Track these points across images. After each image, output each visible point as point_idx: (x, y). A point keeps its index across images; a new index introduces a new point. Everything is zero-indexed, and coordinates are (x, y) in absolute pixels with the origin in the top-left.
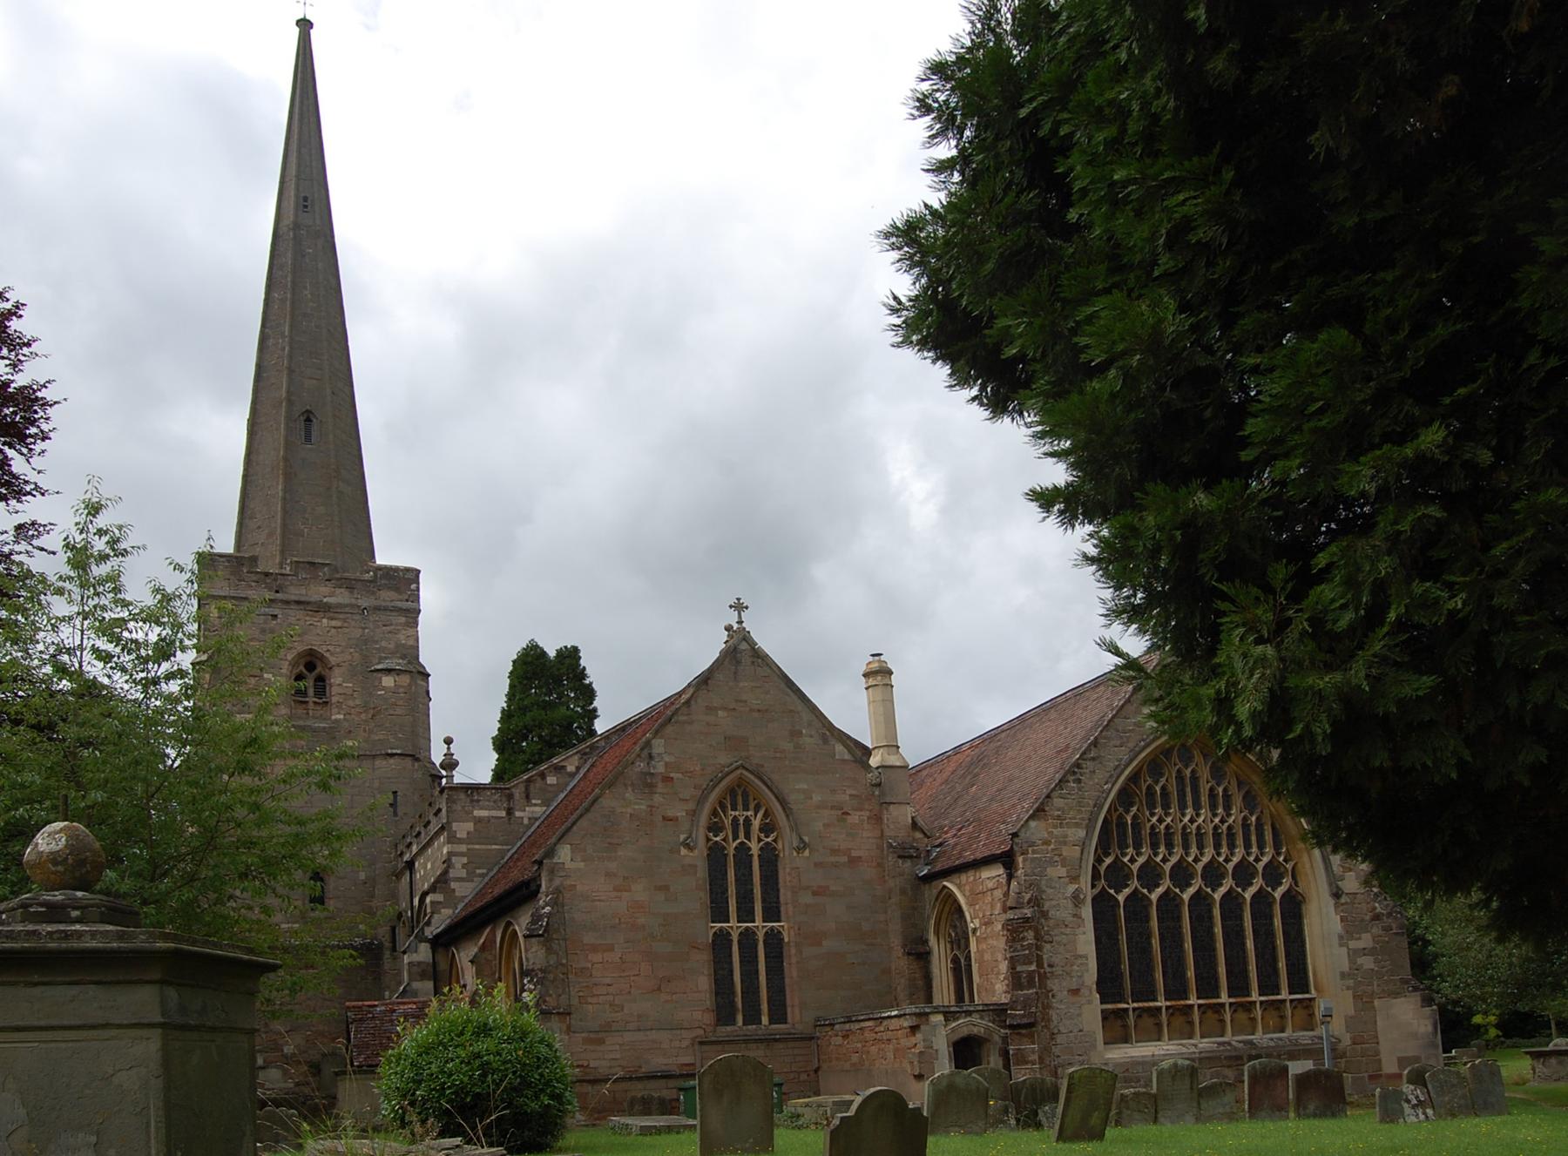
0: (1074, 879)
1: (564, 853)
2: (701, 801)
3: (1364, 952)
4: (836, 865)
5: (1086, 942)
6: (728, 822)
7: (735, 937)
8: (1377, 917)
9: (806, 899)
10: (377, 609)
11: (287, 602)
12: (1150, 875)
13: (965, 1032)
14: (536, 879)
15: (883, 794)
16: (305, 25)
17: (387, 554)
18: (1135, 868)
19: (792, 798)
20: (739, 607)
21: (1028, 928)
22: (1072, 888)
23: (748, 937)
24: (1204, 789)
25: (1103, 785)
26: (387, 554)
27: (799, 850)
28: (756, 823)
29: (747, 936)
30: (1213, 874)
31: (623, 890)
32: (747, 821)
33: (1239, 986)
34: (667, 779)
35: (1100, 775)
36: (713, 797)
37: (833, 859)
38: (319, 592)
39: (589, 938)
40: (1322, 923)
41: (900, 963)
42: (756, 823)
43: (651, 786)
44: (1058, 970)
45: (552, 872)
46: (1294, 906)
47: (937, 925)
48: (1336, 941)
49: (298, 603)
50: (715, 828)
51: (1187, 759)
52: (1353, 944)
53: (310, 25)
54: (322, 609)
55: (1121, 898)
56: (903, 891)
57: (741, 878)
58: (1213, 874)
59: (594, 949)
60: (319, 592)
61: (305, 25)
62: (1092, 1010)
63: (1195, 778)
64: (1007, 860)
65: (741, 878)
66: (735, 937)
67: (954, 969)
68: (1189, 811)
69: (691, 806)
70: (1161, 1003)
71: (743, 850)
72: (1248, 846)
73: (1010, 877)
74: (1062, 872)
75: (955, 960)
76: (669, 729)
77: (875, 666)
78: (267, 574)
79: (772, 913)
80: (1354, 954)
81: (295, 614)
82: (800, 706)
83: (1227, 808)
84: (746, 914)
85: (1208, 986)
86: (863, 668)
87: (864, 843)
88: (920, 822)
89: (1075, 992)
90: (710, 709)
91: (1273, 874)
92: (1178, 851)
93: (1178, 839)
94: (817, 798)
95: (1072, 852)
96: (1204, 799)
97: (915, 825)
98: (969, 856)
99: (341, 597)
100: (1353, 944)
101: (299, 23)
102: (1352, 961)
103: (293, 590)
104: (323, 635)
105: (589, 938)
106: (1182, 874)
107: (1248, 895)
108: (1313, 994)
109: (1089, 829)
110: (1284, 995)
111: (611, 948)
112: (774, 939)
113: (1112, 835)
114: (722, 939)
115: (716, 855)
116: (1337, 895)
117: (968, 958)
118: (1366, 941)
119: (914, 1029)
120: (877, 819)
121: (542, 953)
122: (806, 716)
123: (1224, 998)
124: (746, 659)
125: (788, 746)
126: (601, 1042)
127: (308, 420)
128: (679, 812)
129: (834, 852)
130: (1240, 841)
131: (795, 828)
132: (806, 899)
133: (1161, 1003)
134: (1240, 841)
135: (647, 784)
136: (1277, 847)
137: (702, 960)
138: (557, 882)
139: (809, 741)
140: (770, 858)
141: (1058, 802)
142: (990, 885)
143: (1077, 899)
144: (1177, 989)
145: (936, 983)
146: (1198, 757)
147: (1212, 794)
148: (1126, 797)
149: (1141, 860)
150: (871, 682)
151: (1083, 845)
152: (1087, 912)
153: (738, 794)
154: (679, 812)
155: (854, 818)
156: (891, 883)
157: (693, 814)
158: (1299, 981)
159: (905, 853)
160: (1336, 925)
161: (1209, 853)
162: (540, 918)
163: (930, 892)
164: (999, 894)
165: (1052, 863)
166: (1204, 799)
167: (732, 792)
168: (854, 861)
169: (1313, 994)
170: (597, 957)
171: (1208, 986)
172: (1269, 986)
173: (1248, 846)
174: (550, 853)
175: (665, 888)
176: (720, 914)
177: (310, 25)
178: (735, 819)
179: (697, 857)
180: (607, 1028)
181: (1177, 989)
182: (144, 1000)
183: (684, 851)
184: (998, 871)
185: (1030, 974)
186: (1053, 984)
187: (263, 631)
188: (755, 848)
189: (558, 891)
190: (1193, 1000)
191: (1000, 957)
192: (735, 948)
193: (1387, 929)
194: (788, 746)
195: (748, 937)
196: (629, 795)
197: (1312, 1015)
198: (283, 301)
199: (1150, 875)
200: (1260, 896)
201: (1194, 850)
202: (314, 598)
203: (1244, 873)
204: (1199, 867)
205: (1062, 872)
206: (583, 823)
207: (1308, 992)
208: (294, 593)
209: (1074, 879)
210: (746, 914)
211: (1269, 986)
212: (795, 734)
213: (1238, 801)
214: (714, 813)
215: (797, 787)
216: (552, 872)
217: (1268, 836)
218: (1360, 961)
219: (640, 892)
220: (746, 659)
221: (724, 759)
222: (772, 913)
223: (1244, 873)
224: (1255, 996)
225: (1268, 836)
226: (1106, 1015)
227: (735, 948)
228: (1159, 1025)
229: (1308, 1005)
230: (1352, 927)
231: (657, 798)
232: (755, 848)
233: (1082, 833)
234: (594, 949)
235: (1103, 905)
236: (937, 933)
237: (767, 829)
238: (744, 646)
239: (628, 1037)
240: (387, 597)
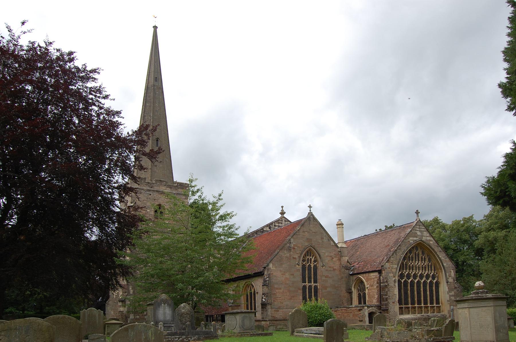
0: (394, 277)
1: (271, 265)
2: (301, 254)
3: (452, 296)
4: (330, 270)
5: (396, 291)
6: (307, 259)
7: (307, 287)
8: (456, 288)
9: (324, 278)
10: (178, 194)
11: (154, 191)
12: (409, 276)
13: (371, 311)
14: (263, 271)
15: (341, 254)
16: (155, 28)
17: (179, 177)
18: (406, 274)
19: (321, 254)
20: (310, 207)
21: (382, 288)
22: (394, 279)
23: (310, 287)
24: (420, 256)
25: (401, 255)
26: (179, 177)
27: (322, 266)
28: (313, 260)
29: (310, 286)
30: (421, 276)
31: (283, 274)
32: (311, 259)
33: (426, 303)
34: (294, 248)
35: (401, 253)
36: (304, 253)
37: (330, 269)
38: (162, 188)
39: (276, 286)
40: (444, 288)
41: (344, 293)
42: (313, 260)
43: (290, 250)
44: (390, 297)
45: (268, 270)
46: (437, 284)
47: (355, 285)
48: (447, 293)
49: (157, 191)
50: (303, 261)
51: (417, 250)
52: (450, 294)
53: (157, 27)
54: (162, 193)
55: (402, 281)
56: (346, 277)
57: (309, 273)
58: (421, 276)
59: (277, 289)
60: (162, 188)
61: (155, 28)
62: (397, 307)
63: (418, 254)
64: (380, 272)
65: (309, 273)
66: (307, 287)
67: (358, 296)
68: (417, 262)
69: (299, 255)
70: (410, 306)
71: (310, 266)
72: (429, 270)
73: (380, 276)
74: (392, 275)
75: (359, 295)
76: (295, 236)
77: (340, 223)
78: (149, 183)
79: (315, 282)
80: (450, 296)
81: (156, 195)
82: (324, 232)
83: (425, 261)
84: (310, 282)
85: (419, 303)
86: (336, 223)
87: (337, 266)
88: (349, 261)
89: (394, 303)
90: (304, 232)
91: (434, 277)
92: (414, 271)
93: (414, 268)
94: (327, 254)
95: (394, 270)
96: (420, 259)
97: (348, 262)
98: (365, 270)
99: (168, 190)
100: (450, 294)
101: (153, 27)
102: (450, 298)
103: (155, 187)
104: (162, 200)
105: (276, 286)
106: (415, 276)
107: (409, 281)
108: (441, 305)
109: (398, 265)
110: (435, 305)
111: (280, 289)
112: (316, 288)
113: (402, 267)
114: (304, 287)
115: (304, 267)
116: (447, 282)
117: (365, 294)
118: (453, 293)
119: (360, 310)
120: (340, 260)
121: (267, 289)
122: (325, 234)
123: (423, 305)
124: (312, 220)
125: (320, 241)
126: (278, 311)
127: (157, 140)
128: (296, 256)
129: (330, 267)
130: (427, 269)
131: (322, 261)
132: (324, 278)
133: (410, 306)
134: (427, 269)
135: (289, 249)
136: (435, 271)
137: (300, 292)
138: (269, 272)
139: (325, 240)
140: (315, 268)
141: (392, 259)
142: (373, 277)
143: (395, 281)
144: (413, 303)
145: (353, 300)
146: (419, 249)
147: (422, 258)
148: (404, 258)
149: (407, 273)
150: (339, 226)
151: (397, 269)
152: (397, 284)
153: (309, 253)
154: (296, 256)
155: (335, 259)
156: (343, 275)
157: (300, 257)
158: (438, 302)
159: (347, 268)
160: (447, 289)
161: (421, 271)
162: (266, 281)
163: (355, 277)
164: (376, 279)
165: (390, 273)
166: (420, 259)
167: (307, 252)
168: (334, 270)
169: (441, 305)
170: (277, 291)
171: (419, 303)
172: (432, 303)
173: (429, 270)
174: (268, 265)
175: (293, 275)
176: (304, 281)
177: (157, 27)
178: (308, 259)
179: (300, 267)
180: (279, 308)
181: (413, 303)
182: (491, 303)
183: (297, 266)
184: (377, 274)
185: (382, 298)
186: (389, 301)
187: (147, 198)
188: (312, 265)
189: (269, 275)
190: (416, 305)
191: (375, 294)
192: (307, 289)
193: (458, 291)
194: (320, 241)
195: (310, 287)
196: (285, 252)
197: (440, 310)
198: (150, 106)
199: (409, 276)
200: (431, 282)
201: (418, 271)
202: (161, 190)
203: (428, 277)
204: (419, 275)
205: (392, 275)
206: (275, 258)
207: (439, 304)
208: (156, 188)
209: (394, 277)
210: (310, 282)
211: (432, 303)
212: (322, 238)
213: (427, 260)
214: (304, 257)
215: (322, 251)
216: (268, 270)
217: (433, 268)
218: (451, 298)
219: (287, 275)
220: (312, 220)
221: (306, 244)
222: (315, 282)
223: (428, 277)
224: (429, 305)
225: (433, 268)
226: (400, 308)
227: (307, 289)
228: (409, 311)
229: (439, 307)
230: (450, 290)
231: (292, 253)
232: (312, 265)
233: (396, 266)
234: (277, 289)
235: (399, 282)
236: (354, 287)
237: (315, 261)
238: (312, 217)
239: (284, 310)
240: (180, 191)
